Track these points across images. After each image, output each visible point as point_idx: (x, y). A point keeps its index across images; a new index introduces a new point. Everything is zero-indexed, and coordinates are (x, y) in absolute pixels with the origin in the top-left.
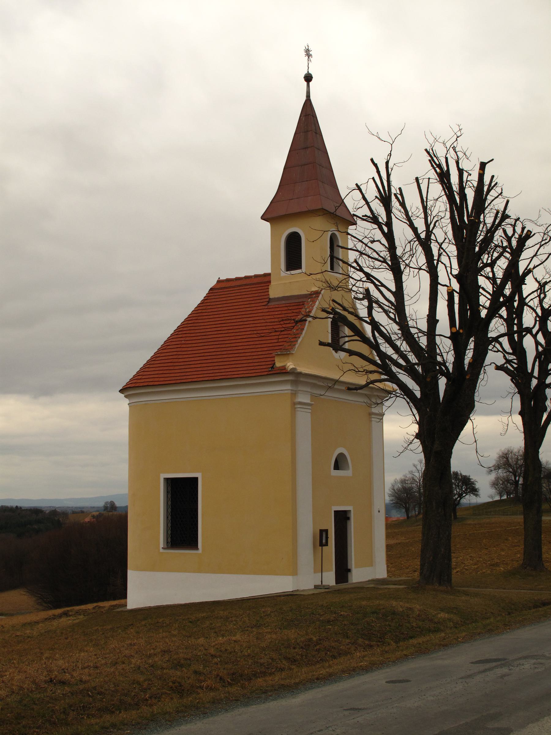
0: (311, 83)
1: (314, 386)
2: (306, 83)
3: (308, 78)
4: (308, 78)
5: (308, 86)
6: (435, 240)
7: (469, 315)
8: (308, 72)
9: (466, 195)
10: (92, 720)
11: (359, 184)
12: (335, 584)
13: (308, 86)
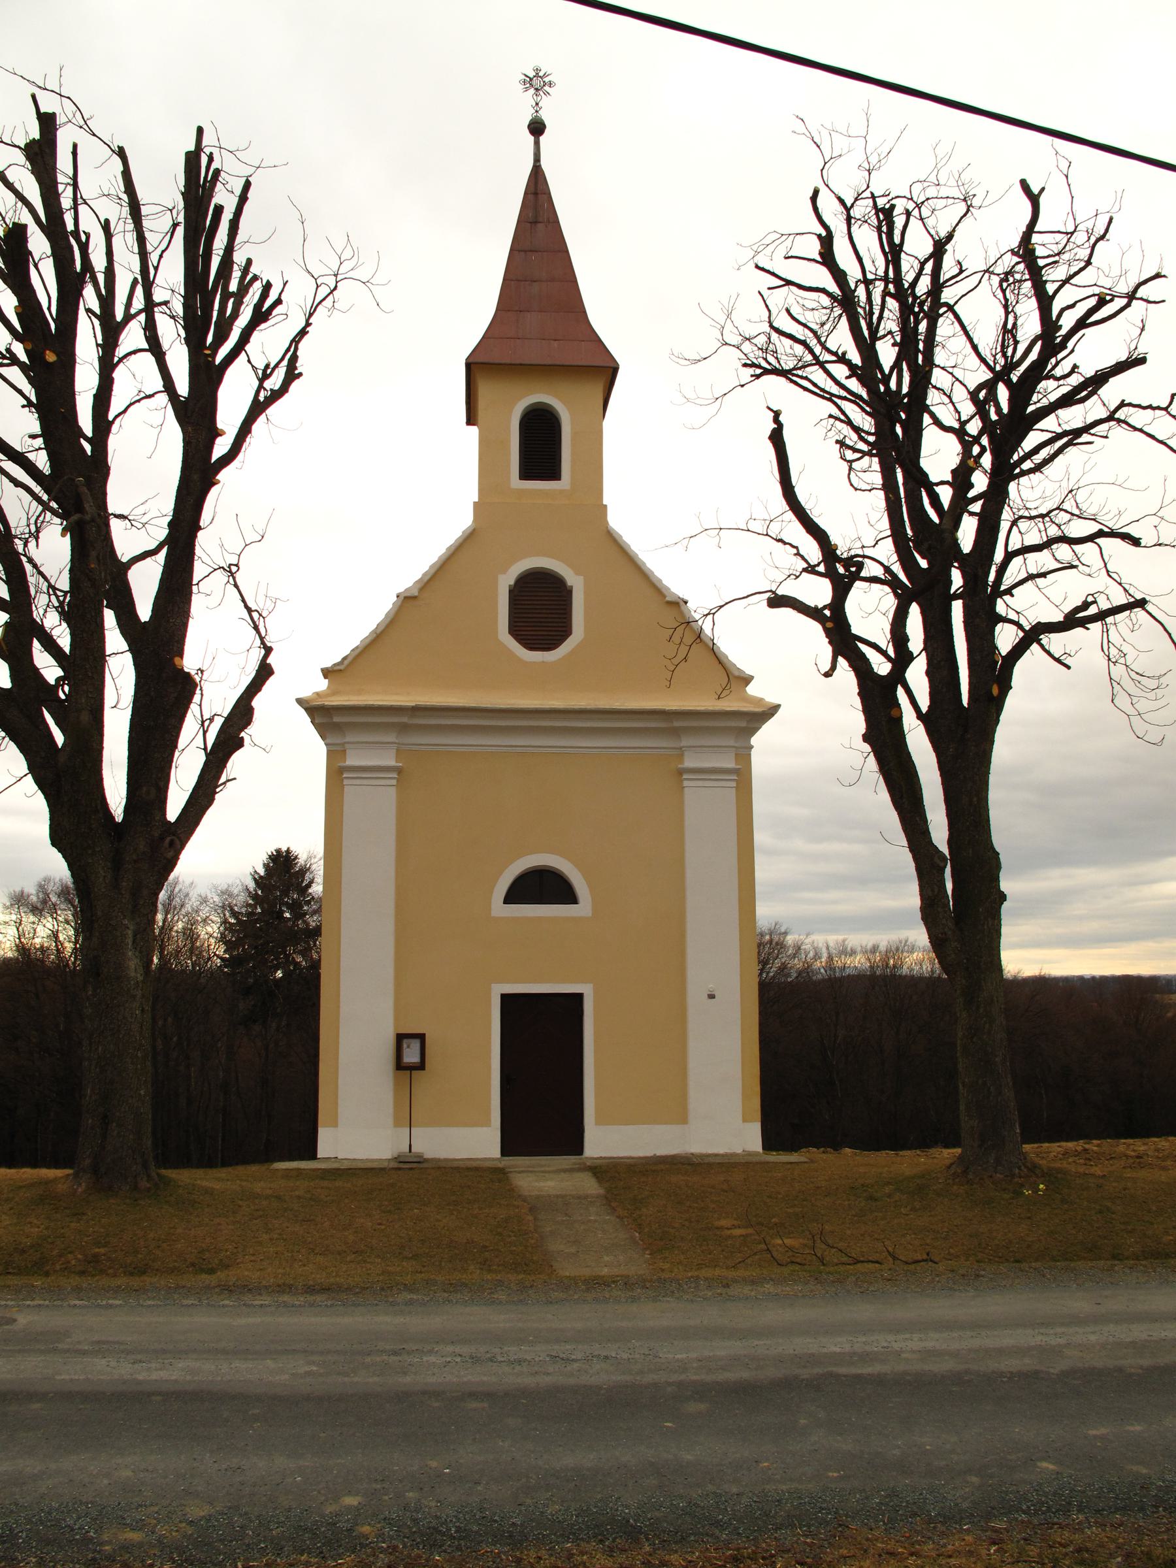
0: (541, 138)
1: (404, 728)
2: (532, 138)
3: (537, 128)
4: (537, 128)
5: (537, 144)
6: (784, 283)
7: (902, 495)
8: (1028, 573)
9: (249, 342)
10: (124, 884)
11: (753, 373)
12: (498, 1155)
13: (537, 144)
